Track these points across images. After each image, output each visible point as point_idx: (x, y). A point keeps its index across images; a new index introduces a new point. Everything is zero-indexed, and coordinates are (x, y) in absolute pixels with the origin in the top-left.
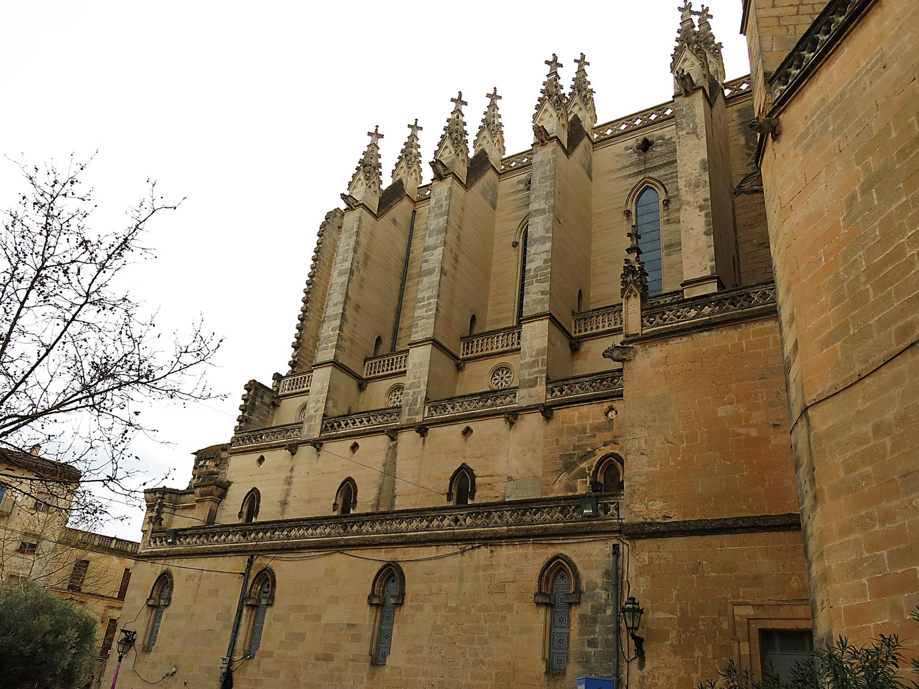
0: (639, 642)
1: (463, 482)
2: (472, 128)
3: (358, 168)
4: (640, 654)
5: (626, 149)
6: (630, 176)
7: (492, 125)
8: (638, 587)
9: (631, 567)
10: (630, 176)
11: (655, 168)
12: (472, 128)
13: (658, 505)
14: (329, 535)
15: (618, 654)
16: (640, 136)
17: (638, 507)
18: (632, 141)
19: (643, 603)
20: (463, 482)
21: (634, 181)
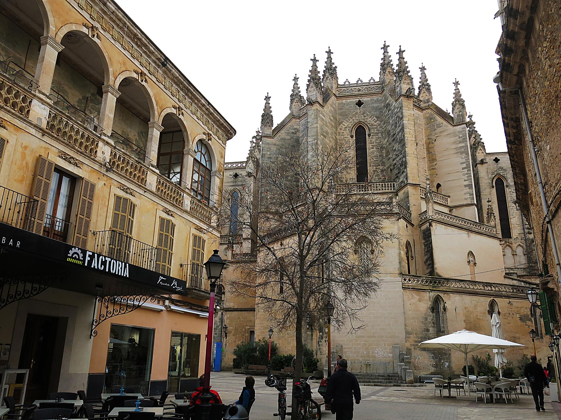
0: (226, 333)
1: (43, 135)
2: (395, 61)
3: (309, 81)
4: (226, 336)
5: (230, 175)
6: (231, 186)
7: (512, 7)
8: (226, 322)
9: (225, 318)
10: (231, 186)
11: (238, 185)
12: (395, 61)
13: (232, 304)
14: (481, 289)
15: (221, 336)
16: (235, 171)
17: (228, 304)
18: (232, 173)
19: (227, 326)
20: (43, 135)
21: (232, 188)
